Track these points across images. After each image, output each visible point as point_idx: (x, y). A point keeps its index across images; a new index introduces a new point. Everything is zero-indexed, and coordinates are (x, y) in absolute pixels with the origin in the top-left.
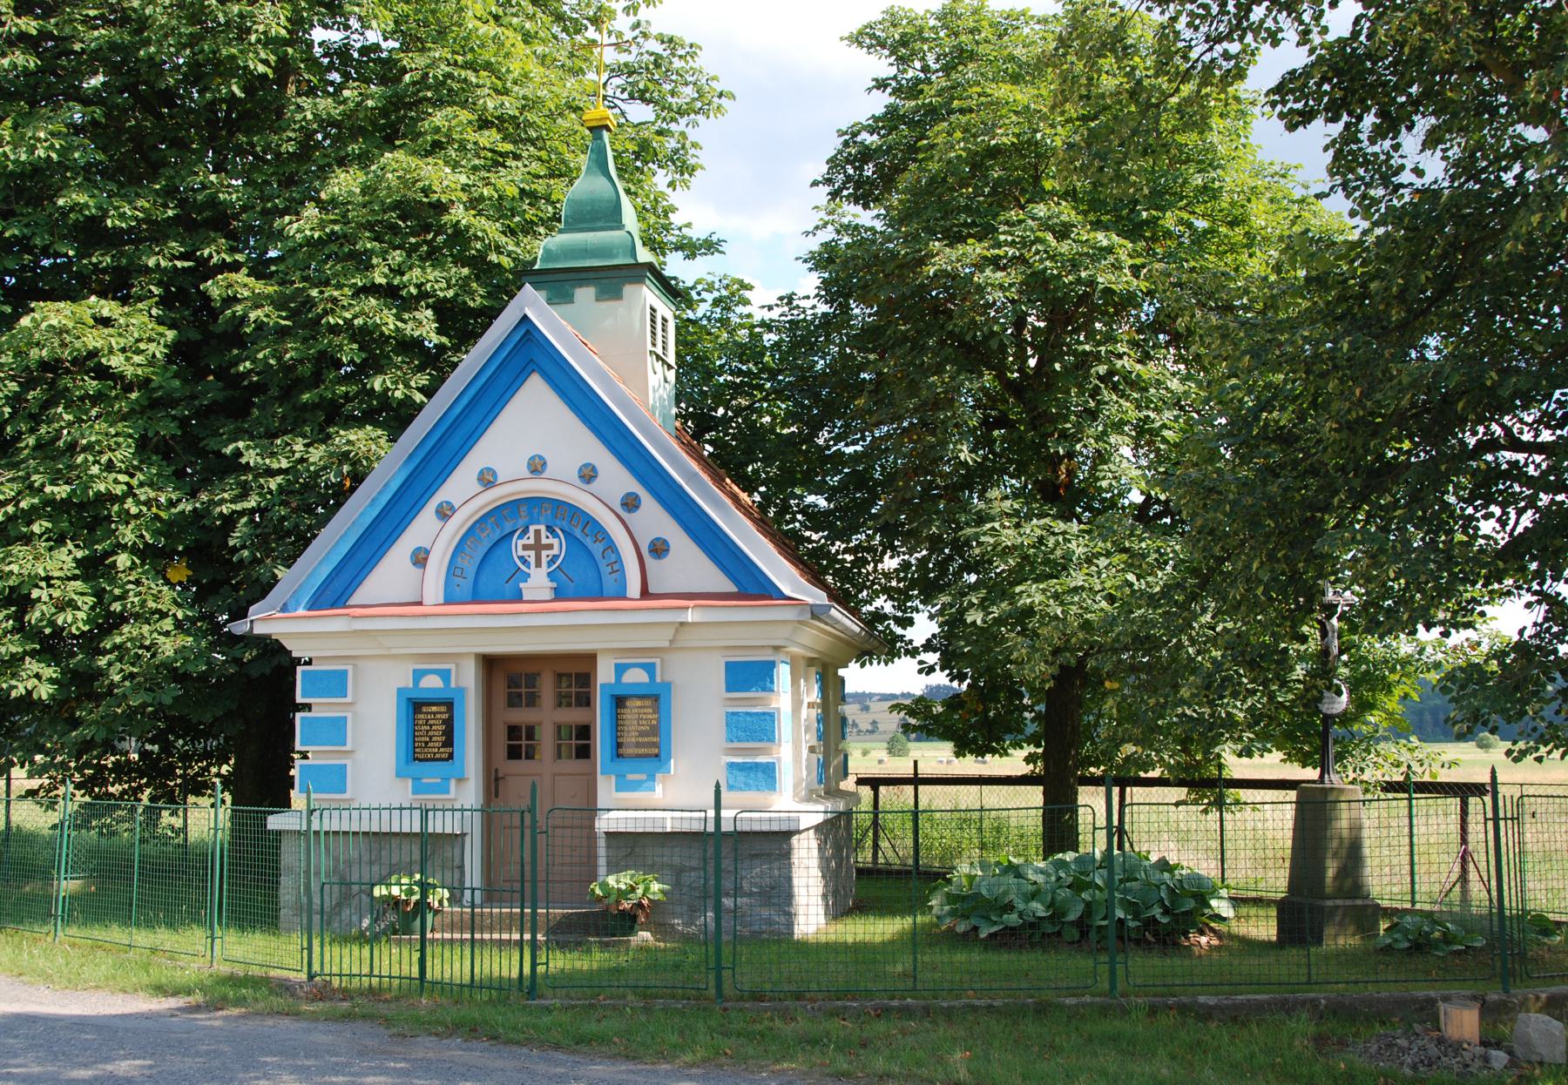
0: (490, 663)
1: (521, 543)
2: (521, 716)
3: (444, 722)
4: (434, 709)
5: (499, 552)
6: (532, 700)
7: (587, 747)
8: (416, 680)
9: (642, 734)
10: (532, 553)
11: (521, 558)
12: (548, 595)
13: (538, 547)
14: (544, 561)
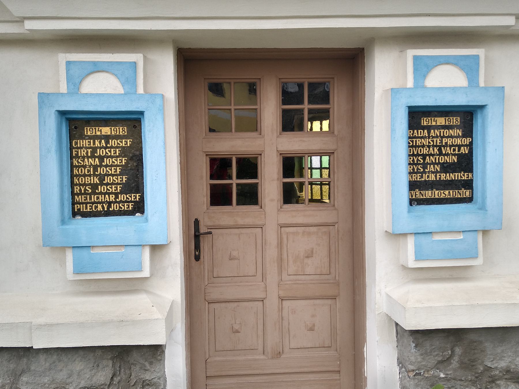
3: (124, 152)
4: (106, 130)
8: (75, 84)
9: (446, 168)
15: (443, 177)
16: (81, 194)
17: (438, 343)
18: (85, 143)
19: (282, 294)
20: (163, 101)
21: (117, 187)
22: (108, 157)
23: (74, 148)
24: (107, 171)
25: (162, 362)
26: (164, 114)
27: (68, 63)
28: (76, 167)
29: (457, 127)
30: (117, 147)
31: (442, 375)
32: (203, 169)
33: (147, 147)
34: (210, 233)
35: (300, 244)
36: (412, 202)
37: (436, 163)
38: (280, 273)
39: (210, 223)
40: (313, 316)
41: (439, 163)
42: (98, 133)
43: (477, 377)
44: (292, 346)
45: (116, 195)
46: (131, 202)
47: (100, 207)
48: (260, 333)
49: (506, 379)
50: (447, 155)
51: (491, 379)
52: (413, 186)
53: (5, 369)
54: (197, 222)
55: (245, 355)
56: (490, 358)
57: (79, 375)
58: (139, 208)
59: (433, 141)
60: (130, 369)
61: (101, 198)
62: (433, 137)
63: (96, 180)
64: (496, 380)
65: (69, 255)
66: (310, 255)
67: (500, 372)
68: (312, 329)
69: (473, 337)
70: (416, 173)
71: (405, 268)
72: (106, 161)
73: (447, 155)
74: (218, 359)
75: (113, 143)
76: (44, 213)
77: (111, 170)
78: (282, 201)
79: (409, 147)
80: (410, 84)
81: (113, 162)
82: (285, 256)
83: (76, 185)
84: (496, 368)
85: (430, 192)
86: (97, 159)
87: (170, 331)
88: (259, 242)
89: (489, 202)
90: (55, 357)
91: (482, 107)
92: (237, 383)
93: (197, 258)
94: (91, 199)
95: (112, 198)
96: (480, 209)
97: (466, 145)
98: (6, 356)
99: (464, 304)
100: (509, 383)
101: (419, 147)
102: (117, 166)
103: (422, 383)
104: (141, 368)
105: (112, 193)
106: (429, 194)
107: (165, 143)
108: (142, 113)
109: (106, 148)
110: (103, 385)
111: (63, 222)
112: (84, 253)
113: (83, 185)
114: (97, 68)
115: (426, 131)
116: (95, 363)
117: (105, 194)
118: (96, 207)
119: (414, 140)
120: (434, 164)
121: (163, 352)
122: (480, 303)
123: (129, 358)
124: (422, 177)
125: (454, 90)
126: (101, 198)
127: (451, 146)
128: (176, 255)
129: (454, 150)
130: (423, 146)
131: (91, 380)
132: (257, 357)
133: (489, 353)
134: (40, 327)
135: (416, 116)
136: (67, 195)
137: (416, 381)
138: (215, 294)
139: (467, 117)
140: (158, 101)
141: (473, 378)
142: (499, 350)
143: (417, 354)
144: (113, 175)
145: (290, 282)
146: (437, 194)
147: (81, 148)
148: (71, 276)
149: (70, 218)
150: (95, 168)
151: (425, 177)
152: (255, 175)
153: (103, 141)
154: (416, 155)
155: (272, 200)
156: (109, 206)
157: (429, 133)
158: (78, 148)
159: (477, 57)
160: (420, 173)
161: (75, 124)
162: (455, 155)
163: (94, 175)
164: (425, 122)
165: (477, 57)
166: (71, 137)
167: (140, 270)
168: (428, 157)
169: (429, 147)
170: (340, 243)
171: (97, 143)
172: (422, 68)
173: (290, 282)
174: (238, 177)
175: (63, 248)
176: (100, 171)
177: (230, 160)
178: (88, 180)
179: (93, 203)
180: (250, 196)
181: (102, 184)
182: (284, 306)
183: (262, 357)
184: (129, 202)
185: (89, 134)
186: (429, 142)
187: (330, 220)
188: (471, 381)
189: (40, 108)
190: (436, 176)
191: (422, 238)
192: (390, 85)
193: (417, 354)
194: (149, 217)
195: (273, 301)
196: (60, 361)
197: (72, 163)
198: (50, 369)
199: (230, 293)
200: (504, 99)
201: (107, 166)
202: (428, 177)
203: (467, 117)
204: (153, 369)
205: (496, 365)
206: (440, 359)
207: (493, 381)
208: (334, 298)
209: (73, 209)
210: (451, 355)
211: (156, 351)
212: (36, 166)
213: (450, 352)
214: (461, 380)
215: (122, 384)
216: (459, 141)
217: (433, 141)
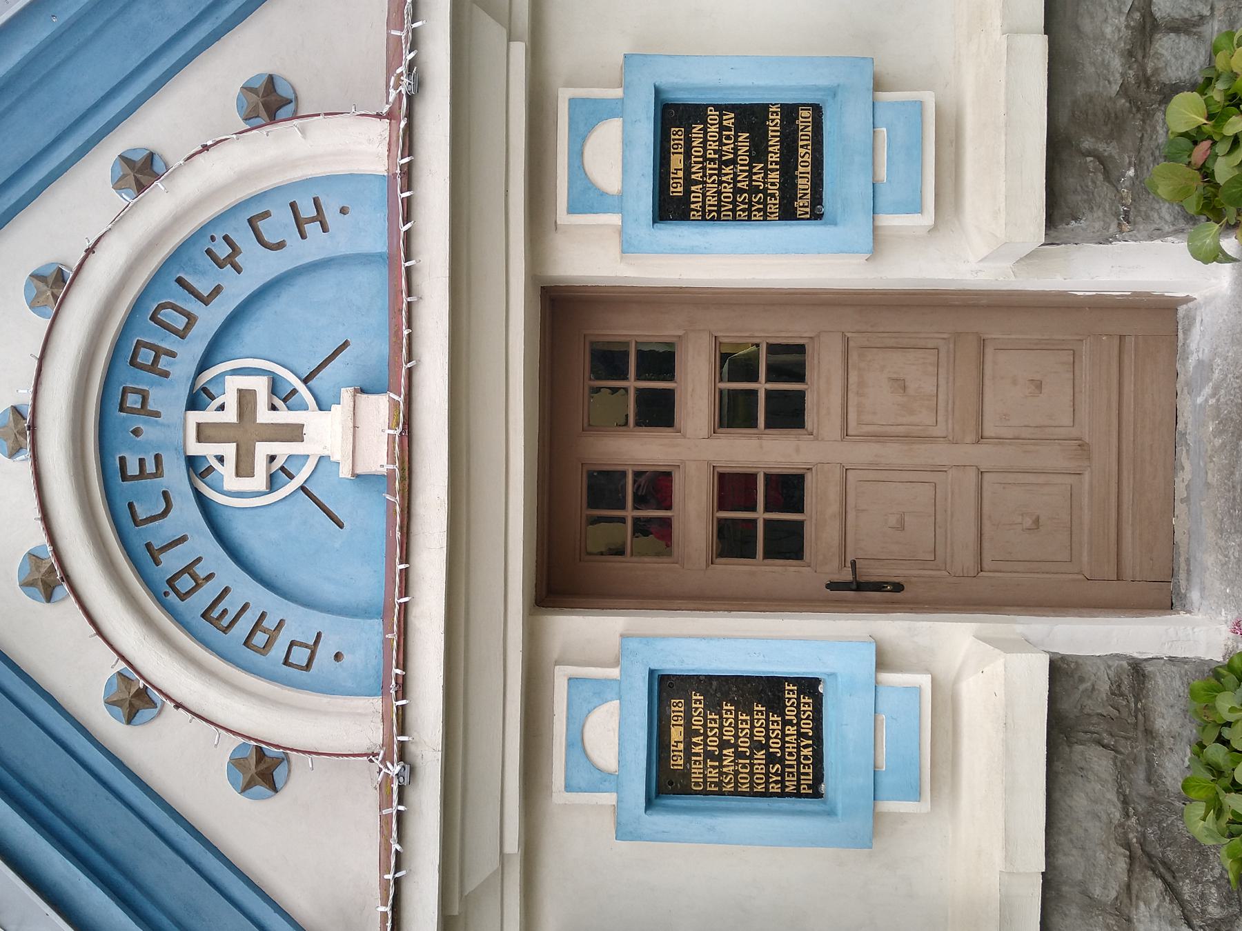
0: (560, 582)
1: (232, 482)
2: (694, 511)
3: (713, 705)
4: (677, 734)
5: (240, 530)
6: (657, 487)
7: (723, 502)
8: (601, 780)
9: (758, 152)
10: (263, 450)
11: (272, 483)
12: (378, 408)
13: (245, 432)
14: (284, 416)
15: (774, 158)
16: (782, 782)
17: (1071, 180)
18: (697, 769)
19: (970, 437)
20: (632, 636)
21: (773, 722)
22: (721, 734)
23: (705, 788)
24: (745, 736)
25: (1080, 661)
26: (655, 637)
27: (568, 788)
28: (736, 786)
29: (688, 132)
30: (705, 717)
31: (1131, 172)
32: (737, 571)
33: (708, 668)
34: (854, 563)
35: (879, 402)
36: (816, 216)
37: (750, 171)
38: (931, 439)
39: (836, 563)
40: (1015, 382)
41: (749, 164)
42: (681, 746)
43: (1138, 110)
44: (1067, 421)
45: (786, 723)
46: (798, 699)
47: (805, 752)
48: (1042, 479)
49: (1144, 57)
50: (736, 149)
51: (1143, 85)
52: (788, 213)
53: (1079, 922)
54: (833, 586)
55: (1081, 509)
56: (1104, 86)
57: (1095, 802)
58: (809, 686)
59: (711, 175)
60: (1088, 714)
61: (790, 748)
62: (704, 175)
63: (760, 754)
64: (1144, 75)
65: (889, 806)
66: (900, 384)
67: (1130, 68)
68: (1039, 385)
69: (1063, 118)
70: (766, 205)
71: (934, 228)
72: (729, 736)
73: (736, 149)
74: (1085, 559)
75: (697, 724)
76: (814, 843)
77: (743, 729)
78: (800, 431)
79: (719, 219)
80: (615, 219)
81: (730, 725)
82: (901, 430)
83: (767, 788)
84: (1122, 75)
85: (800, 181)
86: (725, 752)
87: (1028, 644)
88: (872, 475)
89: (823, 82)
90: (1062, 839)
91: (658, 91)
92: (1132, 525)
93: (898, 587)
94: (791, 766)
95: (791, 730)
96: (835, 95)
97: (721, 116)
98: (1056, 919)
99: (1003, 138)
100: (1152, 52)
101: (719, 200)
102: (736, 719)
103: (1143, 209)
104: (1089, 697)
105: (783, 730)
106: (804, 184)
107: (703, 638)
108: (651, 672)
109: (707, 736)
110: (1115, 764)
111: (831, 813)
112: (886, 781)
113: (768, 778)
114: (576, 743)
115: (693, 188)
116: (1076, 774)
117: (784, 742)
118: (806, 758)
119: (708, 208)
120: (751, 173)
121: (1063, 658)
122: (1003, 111)
123: (1072, 716)
124: (773, 195)
125: (627, 143)
126: (790, 748)
127: (721, 144)
128: (895, 628)
129: (728, 137)
130: (719, 193)
131: (1106, 781)
132: (1086, 486)
133: (1094, 87)
134: (1008, 858)
135: (670, 208)
136: (785, 803)
137: (1139, 219)
138: (964, 558)
139: (674, 116)
140: (633, 644)
141: (1139, 116)
142: (1090, 70)
143: (1090, 217)
144: (753, 727)
145: (950, 421)
146: (804, 169)
147: (705, 777)
148: (924, 806)
149: (825, 803)
150: (739, 755)
151: (774, 190)
152: (750, 478)
153: (694, 740)
154: (735, 206)
155: (798, 450)
156: (805, 736)
157: (696, 183)
158: (705, 782)
159: (572, 101)
160: (765, 199)
161: (667, 783)
162: (736, 136)
163: (751, 757)
164: (677, 190)
165: (572, 101)
166: (686, 791)
167: (919, 690)
168: (739, 185)
169: (720, 183)
170: (882, 329)
171: (696, 750)
172: (588, 198)
173: (950, 421)
174: (766, 522)
175: (876, 816)
176: (744, 747)
177: (720, 520)
178: (759, 769)
179: (799, 763)
180: (788, 489)
181: (766, 746)
182: (993, 435)
183: (1087, 477)
184: (799, 704)
185: (681, 762)
186: (713, 182)
187: (838, 347)
188: (1144, 121)
189: (639, 838)
190: (773, 170)
191: (881, 201)
192: (613, 249)
193: (1090, 217)
194: (827, 670)
195: (983, 455)
196: (1070, 832)
197: (730, 794)
198: (1083, 849)
199: (964, 531)
200: (645, 55)
201: (736, 737)
202: (773, 184)
203: (674, 116)
204: (1093, 678)
205: (1118, 76)
206: (1101, 177)
207: (1147, 81)
208: (983, 343)
209: (807, 796)
210: (1094, 156)
211: (1061, 672)
212: (737, 853)
213: (1089, 159)
214: (1141, 139)
215: (1115, 730)
216: (713, 129)
217: (711, 175)
